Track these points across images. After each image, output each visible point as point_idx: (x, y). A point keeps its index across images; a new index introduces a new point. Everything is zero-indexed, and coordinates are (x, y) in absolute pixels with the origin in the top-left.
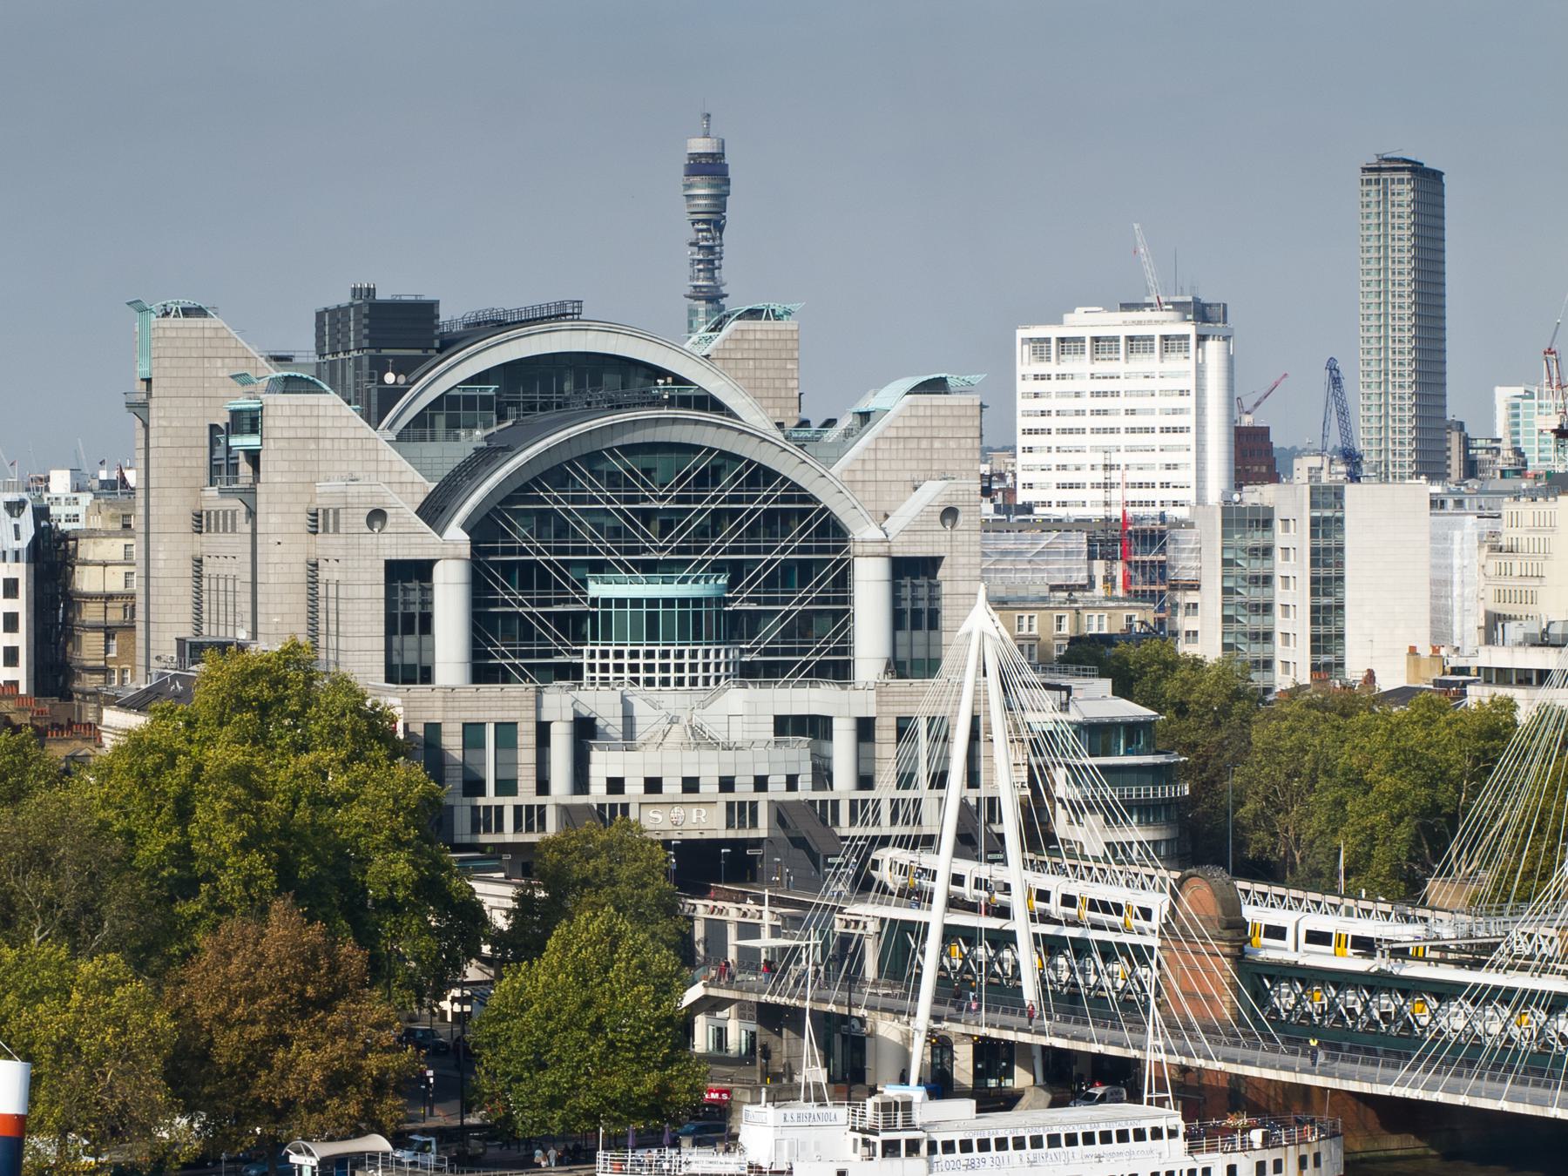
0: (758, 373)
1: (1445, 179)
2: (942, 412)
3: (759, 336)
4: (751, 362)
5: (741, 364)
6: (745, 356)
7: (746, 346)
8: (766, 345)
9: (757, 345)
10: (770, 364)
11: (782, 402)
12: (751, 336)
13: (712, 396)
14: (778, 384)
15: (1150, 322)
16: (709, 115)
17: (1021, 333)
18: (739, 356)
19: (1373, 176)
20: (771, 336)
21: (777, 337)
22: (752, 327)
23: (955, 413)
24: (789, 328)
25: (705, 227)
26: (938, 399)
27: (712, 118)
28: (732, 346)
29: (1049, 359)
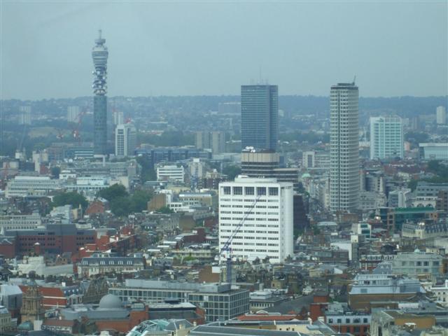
15: (265, 182)
19: (335, 90)
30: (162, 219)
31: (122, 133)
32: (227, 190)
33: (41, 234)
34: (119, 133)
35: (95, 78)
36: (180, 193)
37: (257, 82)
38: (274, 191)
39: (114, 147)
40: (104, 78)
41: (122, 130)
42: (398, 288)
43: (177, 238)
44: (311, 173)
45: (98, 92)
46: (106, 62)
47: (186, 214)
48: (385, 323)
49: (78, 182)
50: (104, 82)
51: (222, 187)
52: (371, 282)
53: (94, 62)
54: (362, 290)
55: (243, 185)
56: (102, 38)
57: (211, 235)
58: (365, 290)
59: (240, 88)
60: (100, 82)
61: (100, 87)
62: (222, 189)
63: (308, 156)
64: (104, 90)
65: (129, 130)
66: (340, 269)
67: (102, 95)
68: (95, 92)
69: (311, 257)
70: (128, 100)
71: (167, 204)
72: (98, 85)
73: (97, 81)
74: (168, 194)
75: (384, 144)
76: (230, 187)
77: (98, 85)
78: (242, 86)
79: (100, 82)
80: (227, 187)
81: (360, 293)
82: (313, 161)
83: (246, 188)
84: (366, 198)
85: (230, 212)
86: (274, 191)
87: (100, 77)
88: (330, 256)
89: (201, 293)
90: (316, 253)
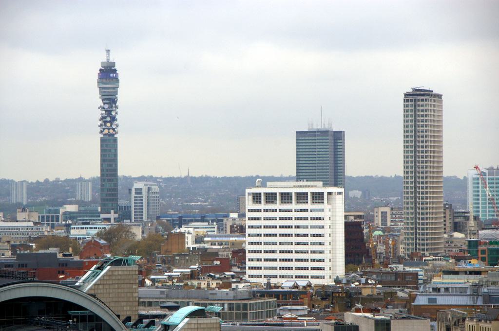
0: (119, 291)
1: (443, 97)
2: (202, 326)
3: (120, 273)
4: (116, 286)
5: (112, 286)
6: (114, 282)
7: (114, 278)
8: (123, 277)
9: (119, 277)
10: (125, 286)
11: (130, 304)
12: (116, 273)
13: (96, 315)
14: (129, 295)
15: (306, 186)
16: (109, 51)
17: (248, 191)
18: (111, 283)
19: (410, 98)
20: (125, 273)
21: (128, 273)
22: (117, 269)
23: (208, 326)
24: (134, 269)
25: (108, 102)
26: (201, 320)
27: (111, 53)
28: (108, 278)
29: (260, 203)
30: (177, 258)
31: (141, 193)
32: (257, 198)
33: (9, 266)
34: (136, 193)
35: (100, 113)
36: (205, 236)
37: (317, 126)
38: (318, 197)
39: (130, 212)
40: (113, 113)
41: (141, 189)
42: (480, 298)
43: (192, 267)
44: (384, 231)
45: (106, 131)
46: (116, 93)
47: (208, 251)
48: (455, 319)
49: (73, 232)
50: (113, 119)
51: (249, 194)
52: (443, 290)
53: (100, 92)
54: (430, 300)
55: (278, 191)
56: (111, 60)
57: (239, 267)
58: (435, 300)
59: (296, 133)
60: (108, 119)
61: (108, 125)
62: (251, 197)
63: (382, 213)
64: (114, 129)
65: (149, 189)
66: (406, 293)
67: (113, 135)
68: (101, 132)
69: (367, 279)
70: (158, 180)
71: (186, 246)
72: (105, 122)
73: (105, 118)
74: (189, 233)
75: (488, 205)
76: (260, 194)
77: (105, 122)
78: (297, 132)
79: (108, 119)
80: (257, 194)
81: (427, 303)
82: (389, 219)
83: (282, 194)
84: (453, 245)
85: (260, 227)
86: (318, 197)
87: (109, 112)
88: (393, 278)
89: (211, 300)
90: (374, 276)
